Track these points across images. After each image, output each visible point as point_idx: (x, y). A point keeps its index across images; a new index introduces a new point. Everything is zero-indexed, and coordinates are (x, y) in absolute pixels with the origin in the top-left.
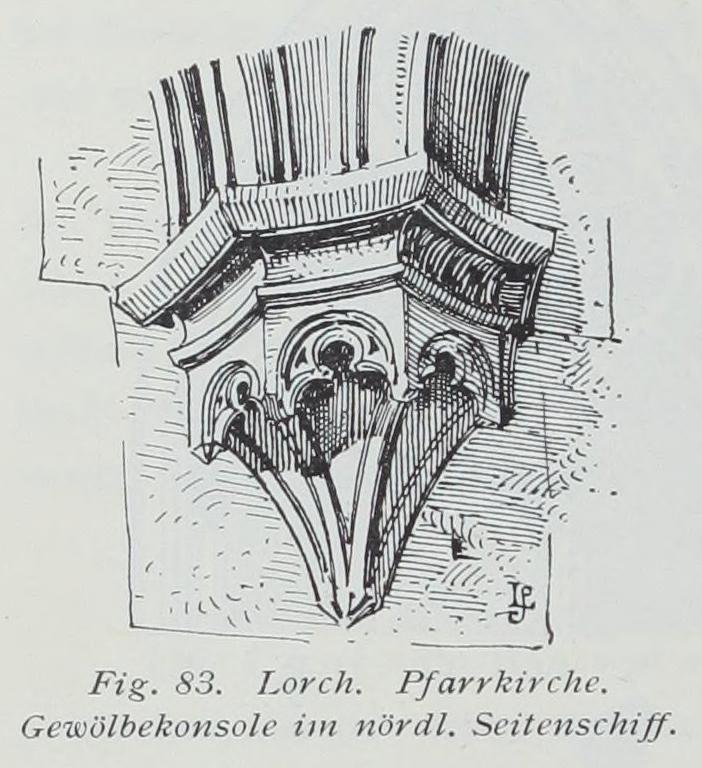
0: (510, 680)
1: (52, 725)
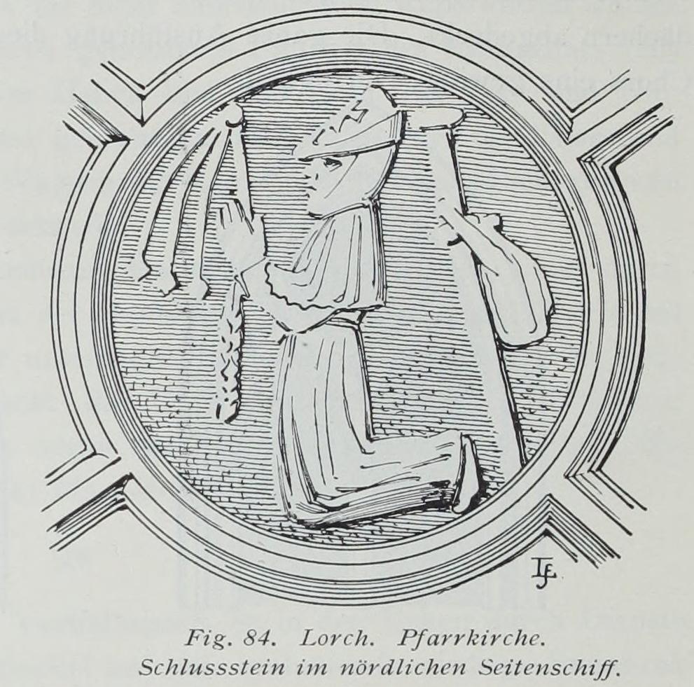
0: (478, 636)
1: (253, 667)
